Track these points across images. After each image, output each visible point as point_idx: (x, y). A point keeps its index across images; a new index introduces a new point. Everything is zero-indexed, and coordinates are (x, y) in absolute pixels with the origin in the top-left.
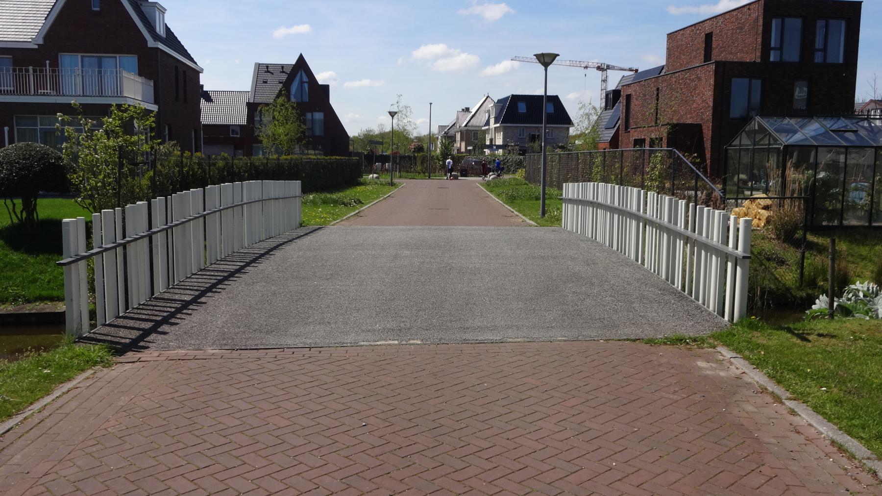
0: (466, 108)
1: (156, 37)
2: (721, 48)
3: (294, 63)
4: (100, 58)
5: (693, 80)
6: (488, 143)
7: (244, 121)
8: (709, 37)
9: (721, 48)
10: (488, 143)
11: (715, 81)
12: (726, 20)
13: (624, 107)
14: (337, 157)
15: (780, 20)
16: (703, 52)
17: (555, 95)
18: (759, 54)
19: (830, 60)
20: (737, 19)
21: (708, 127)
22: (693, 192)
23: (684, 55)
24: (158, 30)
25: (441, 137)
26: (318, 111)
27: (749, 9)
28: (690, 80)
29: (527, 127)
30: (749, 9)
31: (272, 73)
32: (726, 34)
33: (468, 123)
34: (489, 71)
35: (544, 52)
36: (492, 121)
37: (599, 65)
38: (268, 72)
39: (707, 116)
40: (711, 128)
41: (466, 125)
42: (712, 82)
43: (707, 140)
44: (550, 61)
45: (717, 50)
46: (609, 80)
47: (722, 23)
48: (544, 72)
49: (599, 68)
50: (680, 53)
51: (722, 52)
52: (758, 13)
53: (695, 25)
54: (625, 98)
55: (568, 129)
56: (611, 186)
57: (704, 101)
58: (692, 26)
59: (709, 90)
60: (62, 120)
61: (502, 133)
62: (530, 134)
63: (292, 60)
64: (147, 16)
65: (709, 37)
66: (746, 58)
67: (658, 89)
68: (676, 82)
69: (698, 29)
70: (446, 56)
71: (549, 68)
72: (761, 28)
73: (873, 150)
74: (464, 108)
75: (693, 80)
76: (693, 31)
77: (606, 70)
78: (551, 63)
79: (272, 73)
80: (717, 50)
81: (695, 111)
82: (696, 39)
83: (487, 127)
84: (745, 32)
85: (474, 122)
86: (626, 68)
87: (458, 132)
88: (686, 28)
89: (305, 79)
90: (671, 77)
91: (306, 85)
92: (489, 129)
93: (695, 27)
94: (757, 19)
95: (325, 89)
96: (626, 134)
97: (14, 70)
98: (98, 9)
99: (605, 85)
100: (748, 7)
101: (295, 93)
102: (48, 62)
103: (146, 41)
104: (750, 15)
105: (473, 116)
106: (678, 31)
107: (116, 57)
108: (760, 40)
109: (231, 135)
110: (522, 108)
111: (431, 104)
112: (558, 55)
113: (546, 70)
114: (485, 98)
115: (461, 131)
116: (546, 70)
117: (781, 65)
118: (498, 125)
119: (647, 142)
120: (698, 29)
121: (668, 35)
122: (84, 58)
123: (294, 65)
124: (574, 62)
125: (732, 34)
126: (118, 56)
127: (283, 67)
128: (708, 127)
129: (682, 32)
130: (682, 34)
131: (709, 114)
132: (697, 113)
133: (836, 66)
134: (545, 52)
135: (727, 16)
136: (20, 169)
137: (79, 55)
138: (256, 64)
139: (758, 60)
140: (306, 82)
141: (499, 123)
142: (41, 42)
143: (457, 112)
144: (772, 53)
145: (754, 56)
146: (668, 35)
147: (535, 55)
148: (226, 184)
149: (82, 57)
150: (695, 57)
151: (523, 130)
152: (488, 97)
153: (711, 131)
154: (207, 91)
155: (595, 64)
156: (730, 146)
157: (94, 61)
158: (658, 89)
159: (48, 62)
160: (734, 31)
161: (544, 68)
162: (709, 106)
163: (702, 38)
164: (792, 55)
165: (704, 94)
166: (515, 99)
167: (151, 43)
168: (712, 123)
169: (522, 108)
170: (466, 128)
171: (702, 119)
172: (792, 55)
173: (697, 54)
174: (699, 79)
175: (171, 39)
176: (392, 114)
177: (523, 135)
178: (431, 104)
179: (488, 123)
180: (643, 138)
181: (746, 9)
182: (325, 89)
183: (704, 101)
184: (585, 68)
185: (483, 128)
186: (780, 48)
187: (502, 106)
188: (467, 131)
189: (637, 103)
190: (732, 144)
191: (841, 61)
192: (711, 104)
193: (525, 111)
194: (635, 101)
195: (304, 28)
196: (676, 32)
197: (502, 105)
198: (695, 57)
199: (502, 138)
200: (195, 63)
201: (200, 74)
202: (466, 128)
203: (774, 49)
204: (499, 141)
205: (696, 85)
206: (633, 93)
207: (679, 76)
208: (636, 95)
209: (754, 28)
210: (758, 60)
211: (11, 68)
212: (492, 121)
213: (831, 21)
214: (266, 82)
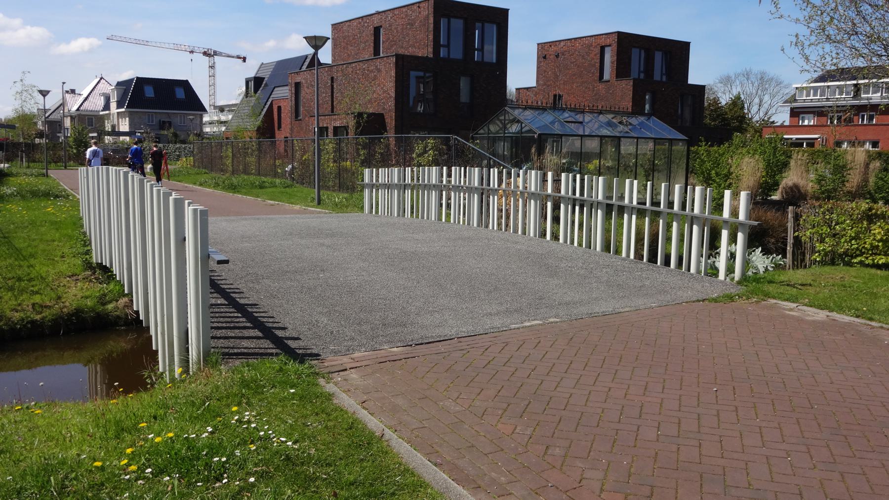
0: (71, 90)
2: (391, 41)
5: (372, 71)
8: (377, 30)
9: (391, 41)
11: (396, 73)
12: (395, 15)
13: (294, 95)
15: (446, 20)
16: (372, 44)
17: (184, 79)
18: (431, 50)
19: (486, 59)
20: (407, 16)
21: (391, 117)
22: (45, 171)
23: (352, 46)
27: (419, 7)
28: (368, 70)
29: (156, 113)
30: (419, 7)
32: (396, 29)
33: (80, 107)
34: (64, 48)
35: (316, 35)
36: (113, 105)
37: (206, 50)
39: (389, 106)
40: (394, 117)
41: (78, 110)
42: (393, 73)
43: (391, 129)
44: (321, 44)
45: (387, 43)
46: (217, 66)
47: (391, 18)
49: (205, 54)
50: (347, 44)
51: (392, 46)
52: (427, 10)
53: (362, 18)
54: (293, 85)
55: (201, 117)
56: (116, 170)
57: (384, 92)
58: (359, 18)
59: (391, 82)
61: (127, 119)
62: (160, 121)
65: (377, 30)
66: (418, 53)
67: (332, 78)
68: (352, 72)
69: (366, 22)
72: (432, 26)
73: (599, 138)
75: (372, 71)
76: (360, 23)
77: (213, 56)
80: (387, 43)
81: (375, 101)
82: (364, 31)
84: (416, 28)
85: (87, 106)
86: (233, 55)
88: (353, 20)
90: (346, 67)
92: (109, 114)
93: (362, 20)
94: (427, 16)
96: (297, 122)
99: (213, 72)
100: (417, 5)
104: (420, 13)
105: (86, 99)
106: (344, 22)
108: (431, 37)
110: (149, 92)
114: (98, 80)
117: (448, 60)
118: (123, 110)
119: (331, 131)
120: (366, 22)
121: (332, 25)
124: (187, 47)
125: (402, 29)
128: (391, 117)
129: (348, 23)
130: (349, 26)
131: (391, 104)
132: (378, 103)
133: (490, 64)
135: (396, 12)
139: (431, 56)
141: (123, 107)
144: (442, 49)
145: (426, 51)
146: (332, 25)
150: (364, 49)
151: (152, 115)
152: (101, 78)
153: (394, 121)
155: (201, 49)
156: (477, 134)
158: (332, 78)
160: (405, 26)
162: (391, 97)
163: (370, 31)
164: (457, 53)
165: (384, 85)
166: (141, 82)
168: (395, 113)
169: (149, 92)
171: (384, 109)
172: (457, 53)
173: (366, 46)
174: (379, 71)
176: (44, 93)
177: (152, 122)
179: (107, 107)
180: (325, 126)
181: (415, 7)
183: (384, 92)
184: (190, 52)
185: (101, 113)
186: (448, 46)
187: (125, 89)
188: (79, 115)
189: (308, 91)
190: (479, 132)
191: (494, 61)
192: (393, 95)
193: (152, 95)
194: (306, 89)
196: (342, 23)
197: (125, 87)
198: (364, 49)
199: (128, 124)
202: (78, 112)
203: (443, 46)
204: (124, 126)
205: (375, 75)
206: (304, 81)
207: (356, 66)
208: (306, 82)
209: (425, 25)
210: (431, 56)
212: (113, 105)
213: (486, 25)
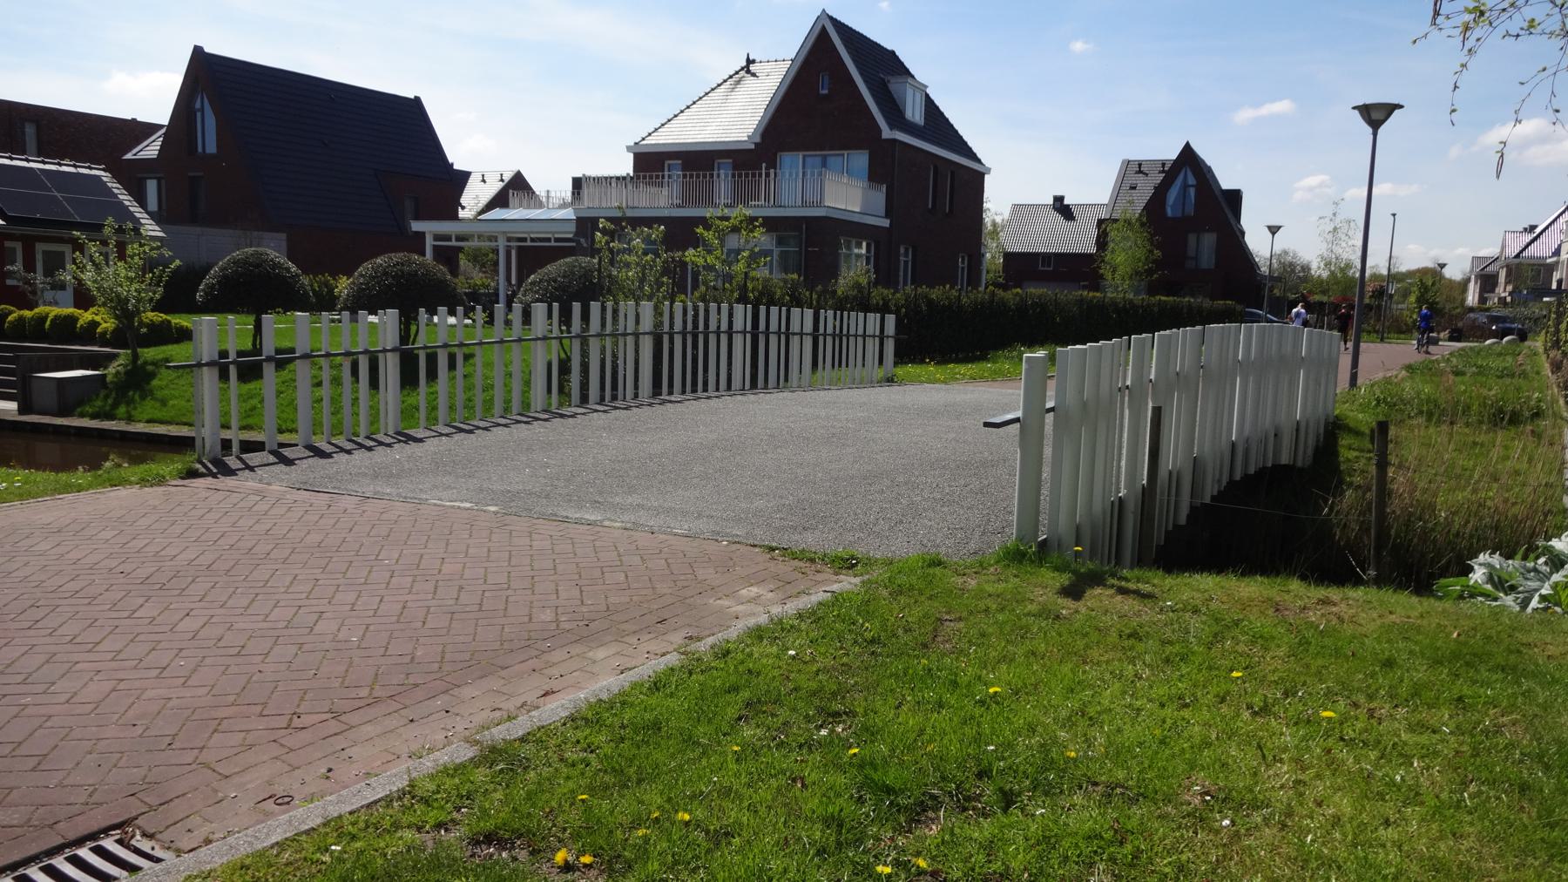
1: (910, 128)
3: (1174, 156)
4: (824, 158)
6: (1554, 286)
7: (1093, 250)
10: (1554, 286)
14: (1163, 298)
24: (909, 114)
25: (1476, 276)
26: (1208, 231)
31: (1147, 175)
38: (1140, 172)
48: (1372, 136)
60: (604, 227)
63: (1172, 154)
64: (895, 96)
70: (1543, 139)
71: (1381, 130)
74: (1526, 226)
78: (1383, 122)
79: (1147, 175)
83: (1554, 259)
87: (1502, 268)
89: (1191, 180)
91: (1192, 191)
92: (1557, 263)
95: (1234, 199)
97: (733, 176)
98: (825, 92)
101: (1175, 201)
102: (764, 165)
103: (879, 131)
107: (843, 155)
109: (1040, 268)
111: (1394, 215)
112: (1402, 107)
113: (1375, 135)
115: (1507, 266)
116: (1375, 135)
122: (808, 159)
123: (1175, 161)
126: (846, 153)
127: (1140, 165)
134: (1368, 102)
136: (555, 289)
137: (801, 155)
138: (1123, 162)
140: (1192, 186)
142: (758, 140)
143: (1503, 233)
147: (1354, 108)
148: (1078, 346)
149: (804, 157)
154: (1068, 206)
157: (818, 160)
159: (764, 165)
161: (1370, 130)
167: (887, 133)
170: (1517, 261)
175: (937, 125)
178: (1394, 215)
182: (1234, 199)
185: (1549, 261)
188: (1519, 265)
195: (1282, 106)
200: (979, 161)
201: (986, 176)
202: (1517, 261)
211: (730, 173)
214: (1134, 188)
